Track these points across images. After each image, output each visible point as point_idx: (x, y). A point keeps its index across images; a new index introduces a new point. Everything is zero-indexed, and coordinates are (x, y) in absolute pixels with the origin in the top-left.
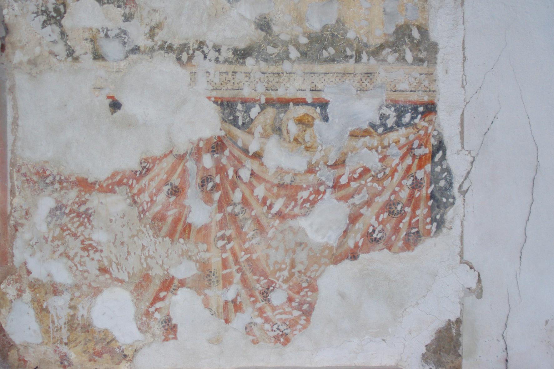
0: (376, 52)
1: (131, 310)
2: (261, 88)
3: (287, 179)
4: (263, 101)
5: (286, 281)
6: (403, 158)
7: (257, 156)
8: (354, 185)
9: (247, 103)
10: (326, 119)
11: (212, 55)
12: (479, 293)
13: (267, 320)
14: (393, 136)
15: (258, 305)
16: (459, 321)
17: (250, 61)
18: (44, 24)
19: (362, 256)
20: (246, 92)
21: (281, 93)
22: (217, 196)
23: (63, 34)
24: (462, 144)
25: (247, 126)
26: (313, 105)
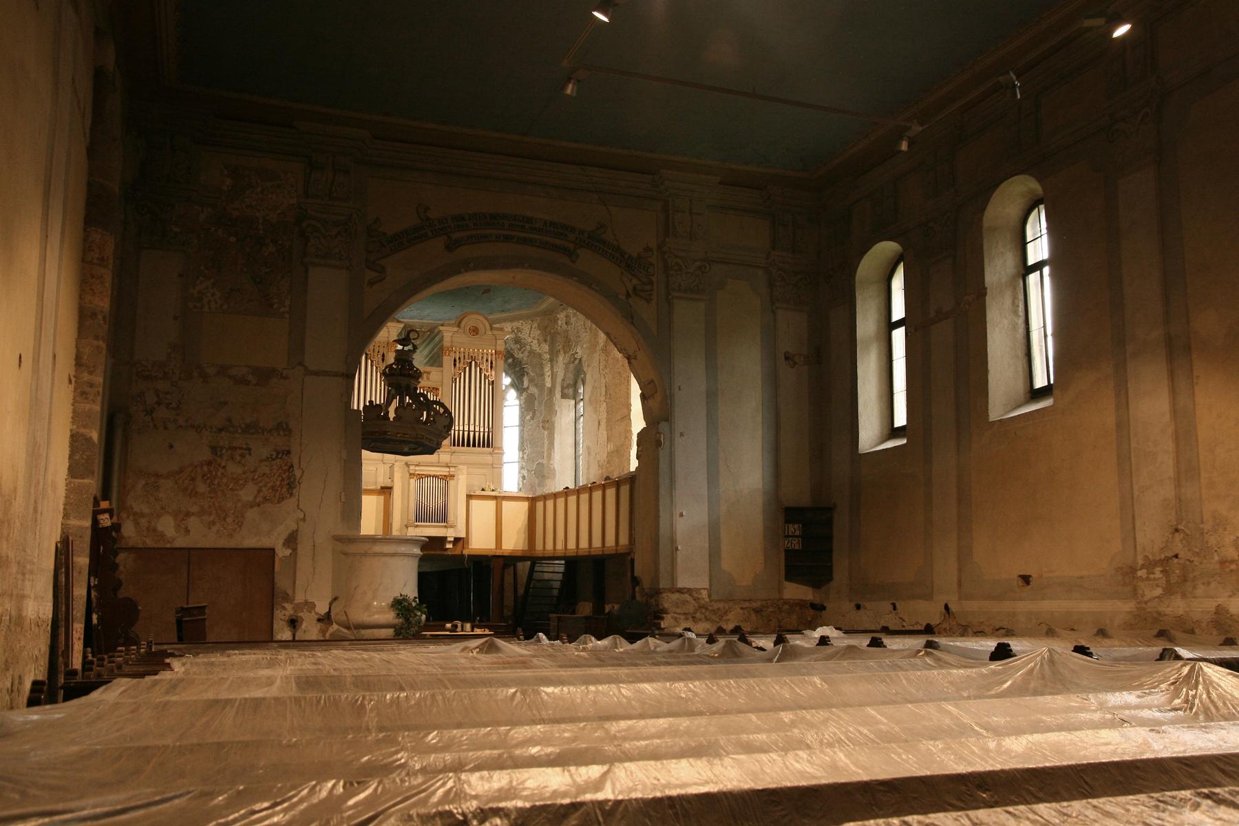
0: (270, 431)
1: (173, 524)
2: (227, 443)
3: (235, 476)
4: (227, 447)
5: (233, 514)
6: (278, 470)
7: (224, 467)
8: (260, 479)
9: (222, 448)
10: (250, 455)
11: (209, 430)
12: (304, 520)
13: (225, 528)
14: (275, 462)
15: (222, 523)
16: (297, 530)
17: (223, 433)
18: (146, 415)
19: (262, 506)
20: (221, 444)
21: (234, 444)
22: (208, 481)
23: (152, 419)
24: (300, 465)
25: (221, 456)
26: (246, 450)
